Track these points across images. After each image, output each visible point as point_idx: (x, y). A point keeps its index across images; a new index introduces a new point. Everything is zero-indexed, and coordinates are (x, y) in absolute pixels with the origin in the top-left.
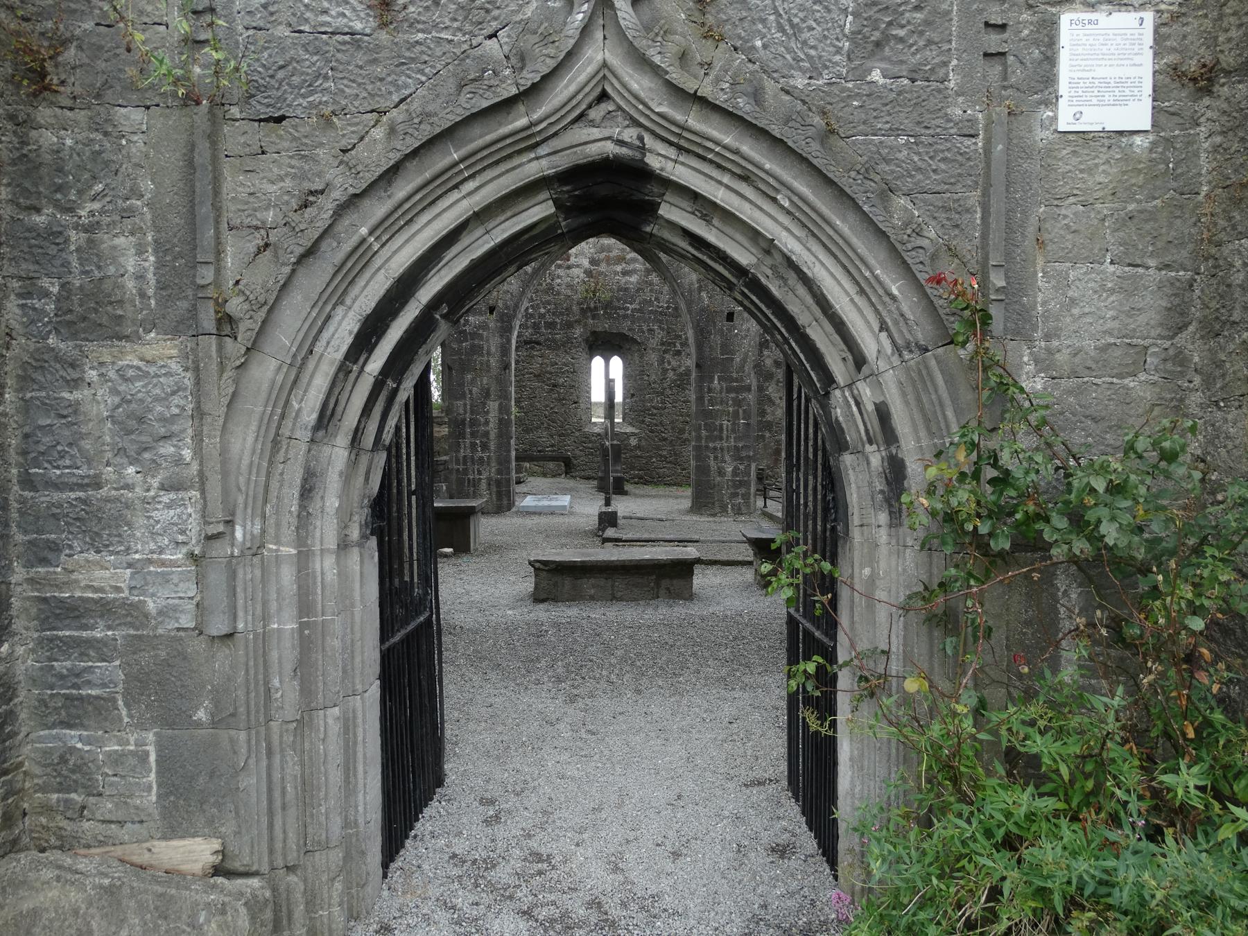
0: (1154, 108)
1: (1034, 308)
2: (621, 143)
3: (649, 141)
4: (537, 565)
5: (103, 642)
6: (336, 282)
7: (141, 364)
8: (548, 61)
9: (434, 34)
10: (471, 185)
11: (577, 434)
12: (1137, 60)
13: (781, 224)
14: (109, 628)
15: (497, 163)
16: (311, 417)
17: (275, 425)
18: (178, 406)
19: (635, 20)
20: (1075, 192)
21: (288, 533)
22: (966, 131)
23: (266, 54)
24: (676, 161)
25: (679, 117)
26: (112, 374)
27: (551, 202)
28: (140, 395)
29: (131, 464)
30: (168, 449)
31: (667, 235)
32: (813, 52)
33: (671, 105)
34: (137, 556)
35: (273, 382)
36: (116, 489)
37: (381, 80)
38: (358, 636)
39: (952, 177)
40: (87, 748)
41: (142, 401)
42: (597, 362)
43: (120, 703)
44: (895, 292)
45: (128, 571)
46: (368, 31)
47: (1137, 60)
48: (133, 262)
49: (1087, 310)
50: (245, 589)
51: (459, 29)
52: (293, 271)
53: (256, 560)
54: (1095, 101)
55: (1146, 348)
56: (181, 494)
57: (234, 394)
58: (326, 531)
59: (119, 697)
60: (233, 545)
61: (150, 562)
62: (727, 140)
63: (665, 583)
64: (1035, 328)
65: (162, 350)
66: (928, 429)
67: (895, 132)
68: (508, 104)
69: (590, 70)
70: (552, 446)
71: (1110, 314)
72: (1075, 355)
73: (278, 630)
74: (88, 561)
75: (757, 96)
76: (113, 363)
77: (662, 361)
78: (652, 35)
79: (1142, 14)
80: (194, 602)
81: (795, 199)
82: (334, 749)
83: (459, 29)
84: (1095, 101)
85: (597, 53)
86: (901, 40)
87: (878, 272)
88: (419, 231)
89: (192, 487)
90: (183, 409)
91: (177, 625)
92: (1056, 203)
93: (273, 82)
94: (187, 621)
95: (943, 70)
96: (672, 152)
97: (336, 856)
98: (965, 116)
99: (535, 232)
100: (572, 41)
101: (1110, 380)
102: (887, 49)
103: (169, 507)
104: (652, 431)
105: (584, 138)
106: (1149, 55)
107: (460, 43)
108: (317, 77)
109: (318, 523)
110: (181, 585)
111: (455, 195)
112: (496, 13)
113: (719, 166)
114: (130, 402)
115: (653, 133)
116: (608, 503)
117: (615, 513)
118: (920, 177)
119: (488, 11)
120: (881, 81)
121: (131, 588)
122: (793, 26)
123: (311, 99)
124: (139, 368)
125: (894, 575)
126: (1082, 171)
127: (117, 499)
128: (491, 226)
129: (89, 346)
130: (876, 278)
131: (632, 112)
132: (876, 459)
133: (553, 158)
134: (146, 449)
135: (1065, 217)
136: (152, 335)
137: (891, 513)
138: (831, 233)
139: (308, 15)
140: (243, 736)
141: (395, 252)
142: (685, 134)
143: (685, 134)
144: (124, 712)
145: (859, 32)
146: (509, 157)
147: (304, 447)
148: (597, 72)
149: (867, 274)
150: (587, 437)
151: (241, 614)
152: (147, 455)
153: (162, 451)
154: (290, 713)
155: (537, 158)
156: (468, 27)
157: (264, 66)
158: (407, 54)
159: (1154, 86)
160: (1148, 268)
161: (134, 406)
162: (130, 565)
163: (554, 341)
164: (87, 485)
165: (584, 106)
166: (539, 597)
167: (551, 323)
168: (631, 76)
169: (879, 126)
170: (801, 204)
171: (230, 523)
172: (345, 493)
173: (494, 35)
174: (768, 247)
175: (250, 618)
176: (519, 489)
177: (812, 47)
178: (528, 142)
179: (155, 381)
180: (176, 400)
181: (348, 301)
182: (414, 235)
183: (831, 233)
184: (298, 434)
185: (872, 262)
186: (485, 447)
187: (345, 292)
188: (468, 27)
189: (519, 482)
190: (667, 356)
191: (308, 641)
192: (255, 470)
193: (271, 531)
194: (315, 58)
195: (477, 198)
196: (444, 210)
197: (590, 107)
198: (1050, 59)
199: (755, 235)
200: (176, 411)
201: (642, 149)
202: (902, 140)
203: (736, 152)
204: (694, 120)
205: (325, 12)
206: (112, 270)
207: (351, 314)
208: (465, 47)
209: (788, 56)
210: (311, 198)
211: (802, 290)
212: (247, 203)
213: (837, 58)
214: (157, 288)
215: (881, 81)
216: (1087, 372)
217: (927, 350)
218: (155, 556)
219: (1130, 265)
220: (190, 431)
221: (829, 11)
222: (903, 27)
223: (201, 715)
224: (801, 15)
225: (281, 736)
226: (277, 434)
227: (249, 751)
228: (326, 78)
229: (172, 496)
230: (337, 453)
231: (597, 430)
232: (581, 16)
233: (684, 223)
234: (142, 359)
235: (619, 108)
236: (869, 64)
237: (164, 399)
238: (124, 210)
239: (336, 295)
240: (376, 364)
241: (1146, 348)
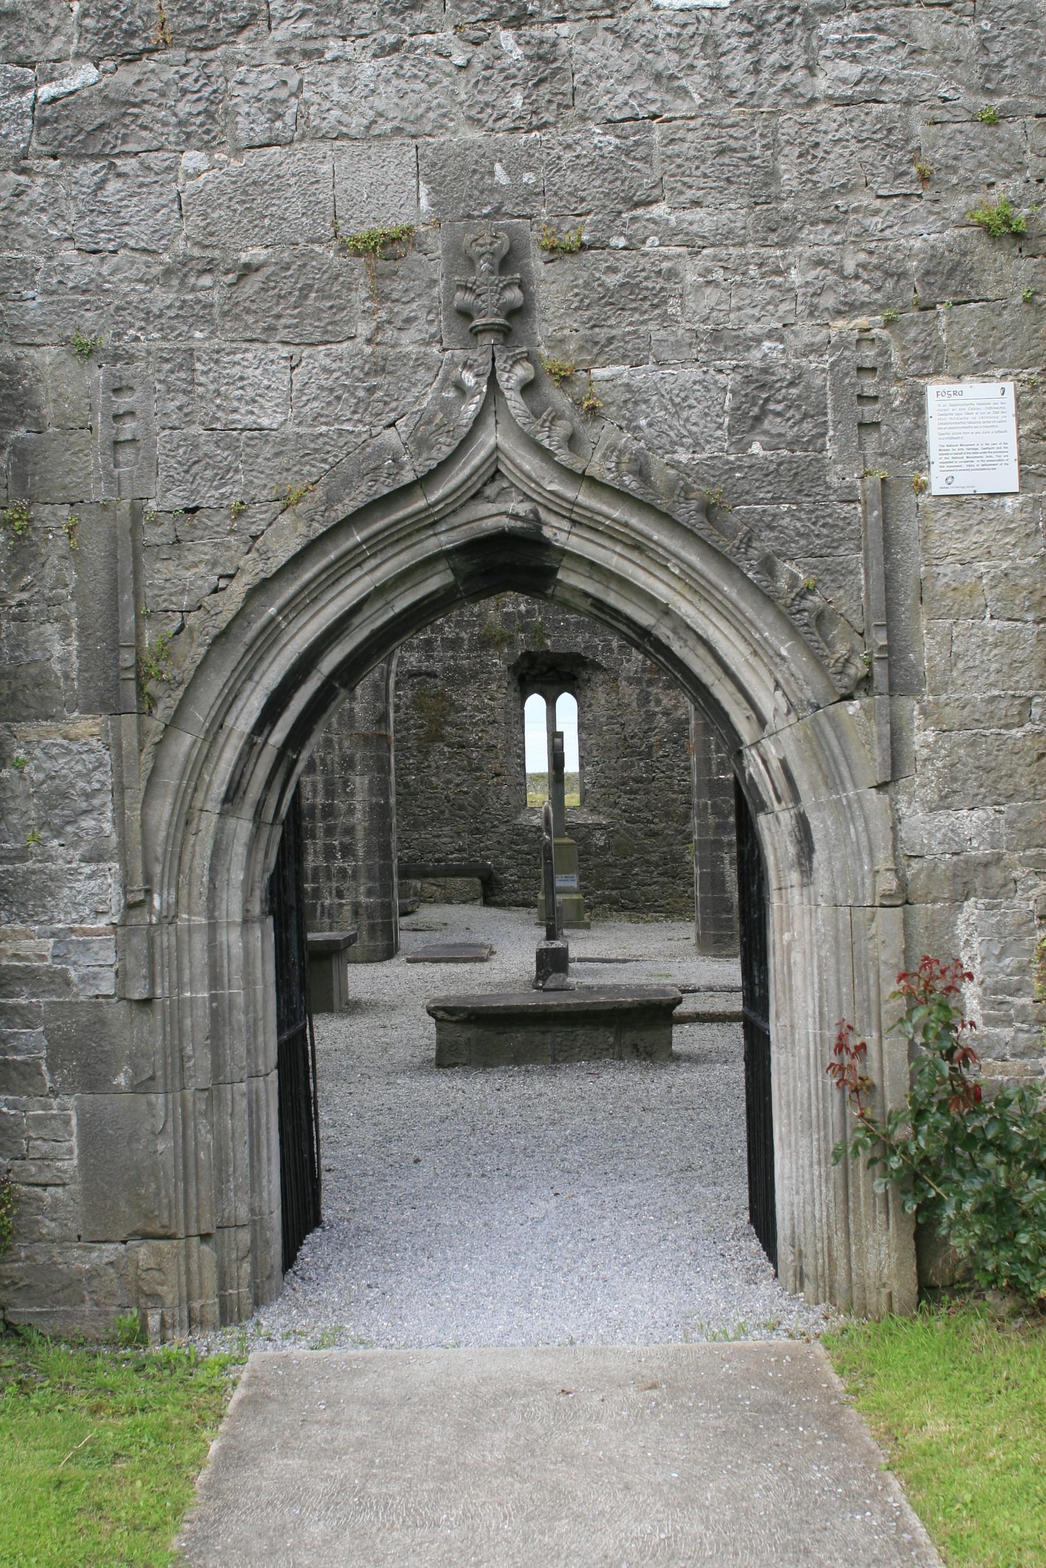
0: (1020, 471)
1: (921, 664)
2: (515, 516)
3: (543, 514)
4: (440, 1014)
5: (29, 1008)
6: (247, 659)
7: (65, 742)
8: (444, 448)
9: (337, 426)
10: (373, 563)
11: (503, 829)
12: (1001, 427)
13: (674, 589)
14: (34, 995)
15: (397, 541)
16: (219, 789)
17: (188, 798)
18: (98, 781)
19: (524, 407)
20: (952, 551)
21: (201, 903)
22: (844, 497)
23: (181, 451)
24: (569, 533)
25: (570, 494)
26: (38, 752)
27: (449, 571)
28: (64, 772)
29: (55, 837)
30: (88, 823)
31: (567, 596)
32: (694, 429)
33: (561, 483)
34: (60, 926)
35: (188, 756)
36: (40, 861)
37: (288, 470)
38: (261, 1015)
39: (833, 541)
40: (12, 1112)
41: (65, 777)
42: (535, 705)
43: (44, 1068)
44: (784, 653)
45: (52, 940)
46: (275, 426)
47: (1001, 427)
48: (59, 649)
49: (971, 664)
50: (162, 956)
51: (360, 421)
52: (208, 651)
53: (171, 928)
54: (964, 466)
55: (1030, 699)
56: (102, 865)
57: (154, 770)
58: (232, 904)
59: (43, 1063)
60: (151, 914)
61: (72, 931)
62: (616, 514)
63: (629, 1037)
64: (922, 683)
65: (87, 726)
66: (827, 784)
67: (776, 500)
68: (405, 491)
69: (483, 454)
70: (460, 850)
71: (994, 666)
72: (964, 707)
73: (191, 998)
74: (14, 931)
75: (642, 473)
76: (39, 742)
77: (644, 699)
78: (540, 421)
79: (1003, 384)
80: (114, 969)
81: (684, 567)
82: (242, 1125)
83: (360, 421)
84: (964, 466)
85: (490, 438)
86: (779, 414)
87: (766, 634)
88: (323, 607)
89: (111, 858)
90: (103, 784)
91: (97, 992)
92: (935, 562)
93: (188, 477)
94: (107, 987)
95: (820, 441)
96: (566, 525)
97: (244, 1237)
98: (844, 483)
99: (436, 596)
100: (466, 430)
101: (998, 731)
102: (766, 422)
103: (90, 877)
104: (633, 821)
105: (480, 515)
106: (1012, 422)
107: (360, 434)
108: (228, 471)
109: (225, 896)
110: (101, 953)
111: (358, 573)
112: (394, 405)
113: (611, 537)
114: (53, 778)
115: (546, 507)
116: (551, 935)
117: (565, 951)
118: (803, 542)
119: (386, 403)
120: (762, 453)
121: (55, 957)
122: (674, 405)
123: (223, 490)
124: (62, 746)
125: (807, 936)
126: (958, 531)
127: (42, 871)
128: (391, 597)
129: (16, 727)
130: (765, 639)
131: (525, 489)
132: (787, 818)
133: (451, 534)
134: (69, 823)
135: (945, 575)
136: (76, 714)
137: (802, 872)
138: (720, 598)
139: (219, 414)
140: (161, 1098)
141: (300, 629)
142: (576, 509)
143: (576, 509)
144: (47, 1077)
145: (739, 409)
146: (410, 535)
147: (214, 818)
148: (491, 455)
149: (757, 636)
150: (521, 833)
151: (158, 980)
152: (69, 829)
153: (84, 824)
154: (202, 1080)
155: (435, 535)
156: (368, 419)
157: (179, 463)
158: (312, 446)
159: (1020, 451)
160: (1026, 622)
161: (57, 781)
162: (53, 935)
163: (459, 670)
164: (15, 858)
165: (479, 486)
166: (447, 1058)
167: (452, 641)
168: (523, 458)
169: (762, 495)
170: (689, 571)
171: (149, 892)
172: (248, 869)
173: (393, 425)
174: (666, 611)
175: (167, 984)
176: (403, 921)
177: (694, 424)
178: (427, 522)
179: (78, 757)
180: (97, 775)
181: (256, 678)
182: (318, 612)
183: (720, 598)
184: (209, 806)
185: (760, 625)
186: (347, 851)
187: (254, 669)
188: (368, 419)
189: (405, 913)
190: (654, 690)
191: (218, 1016)
192: (171, 841)
193: (184, 901)
194: (226, 453)
195: (378, 574)
196: (347, 587)
197: (485, 484)
198: (920, 427)
199: (651, 600)
200: (97, 786)
201: (538, 523)
202: (784, 507)
203: (626, 525)
204: (584, 497)
205: (235, 411)
206: (39, 655)
207: (260, 687)
208: (365, 436)
209: (672, 433)
210: (222, 584)
211: (701, 651)
212: (163, 588)
213: (719, 433)
214: (80, 670)
215: (762, 453)
216: (975, 724)
217: (819, 708)
218: (77, 925)
219: (1009, 619)
220: (110, 806)
221: (709, 390)
222: (779, 402)
223: (121, 1080)
224: (682, 395)
225: (194, 1104)
226: (190, 807)
227: (166, 1115)
228: (237, 471)
229: (93, 867)
230: (242, 827)
231: (537, 821)
232: (473, 407)
233: (582, 586)
234: (65, 738)
235: (513, 485)
236: (748, 437)
237: (87, 776)
238: (50, 599)
239: (247, 672)
240: (278, 736)
241: (1030, 699)
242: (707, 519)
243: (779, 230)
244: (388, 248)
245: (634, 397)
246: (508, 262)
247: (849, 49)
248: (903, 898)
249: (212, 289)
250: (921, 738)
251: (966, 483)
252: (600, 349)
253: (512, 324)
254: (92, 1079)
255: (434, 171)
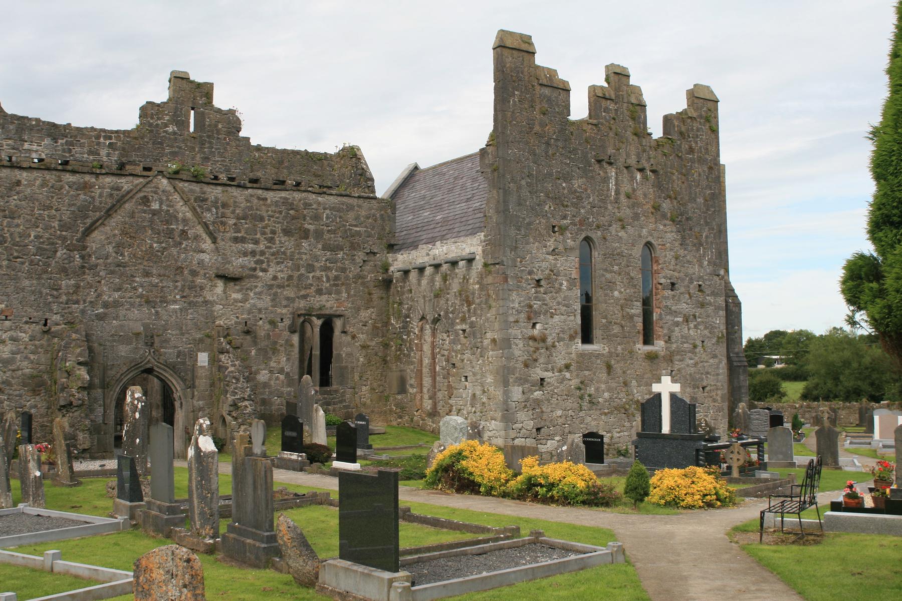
65: (99, 390)
242: (173, 367)
243: (183, 334)
244: (137, 335)
245: (165, 353)
246: (152, 337)
247: (191, 314)
248: (193, 411)
249: (116, 338)
250: (196, 393)
251: (202, 364)
252: (162, 347)
253: (152, 344)
254: (99, 433)
255: (143, 325)
